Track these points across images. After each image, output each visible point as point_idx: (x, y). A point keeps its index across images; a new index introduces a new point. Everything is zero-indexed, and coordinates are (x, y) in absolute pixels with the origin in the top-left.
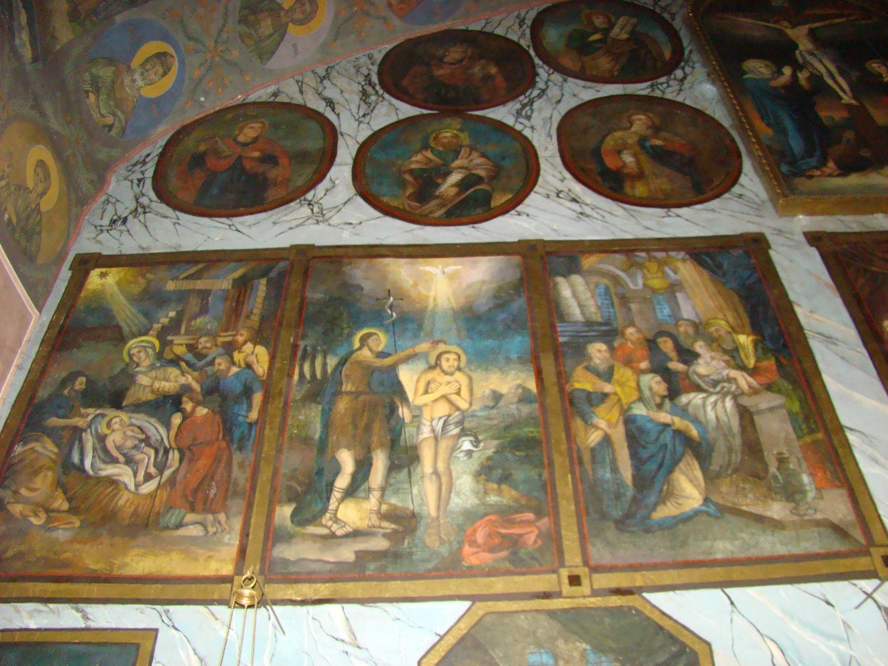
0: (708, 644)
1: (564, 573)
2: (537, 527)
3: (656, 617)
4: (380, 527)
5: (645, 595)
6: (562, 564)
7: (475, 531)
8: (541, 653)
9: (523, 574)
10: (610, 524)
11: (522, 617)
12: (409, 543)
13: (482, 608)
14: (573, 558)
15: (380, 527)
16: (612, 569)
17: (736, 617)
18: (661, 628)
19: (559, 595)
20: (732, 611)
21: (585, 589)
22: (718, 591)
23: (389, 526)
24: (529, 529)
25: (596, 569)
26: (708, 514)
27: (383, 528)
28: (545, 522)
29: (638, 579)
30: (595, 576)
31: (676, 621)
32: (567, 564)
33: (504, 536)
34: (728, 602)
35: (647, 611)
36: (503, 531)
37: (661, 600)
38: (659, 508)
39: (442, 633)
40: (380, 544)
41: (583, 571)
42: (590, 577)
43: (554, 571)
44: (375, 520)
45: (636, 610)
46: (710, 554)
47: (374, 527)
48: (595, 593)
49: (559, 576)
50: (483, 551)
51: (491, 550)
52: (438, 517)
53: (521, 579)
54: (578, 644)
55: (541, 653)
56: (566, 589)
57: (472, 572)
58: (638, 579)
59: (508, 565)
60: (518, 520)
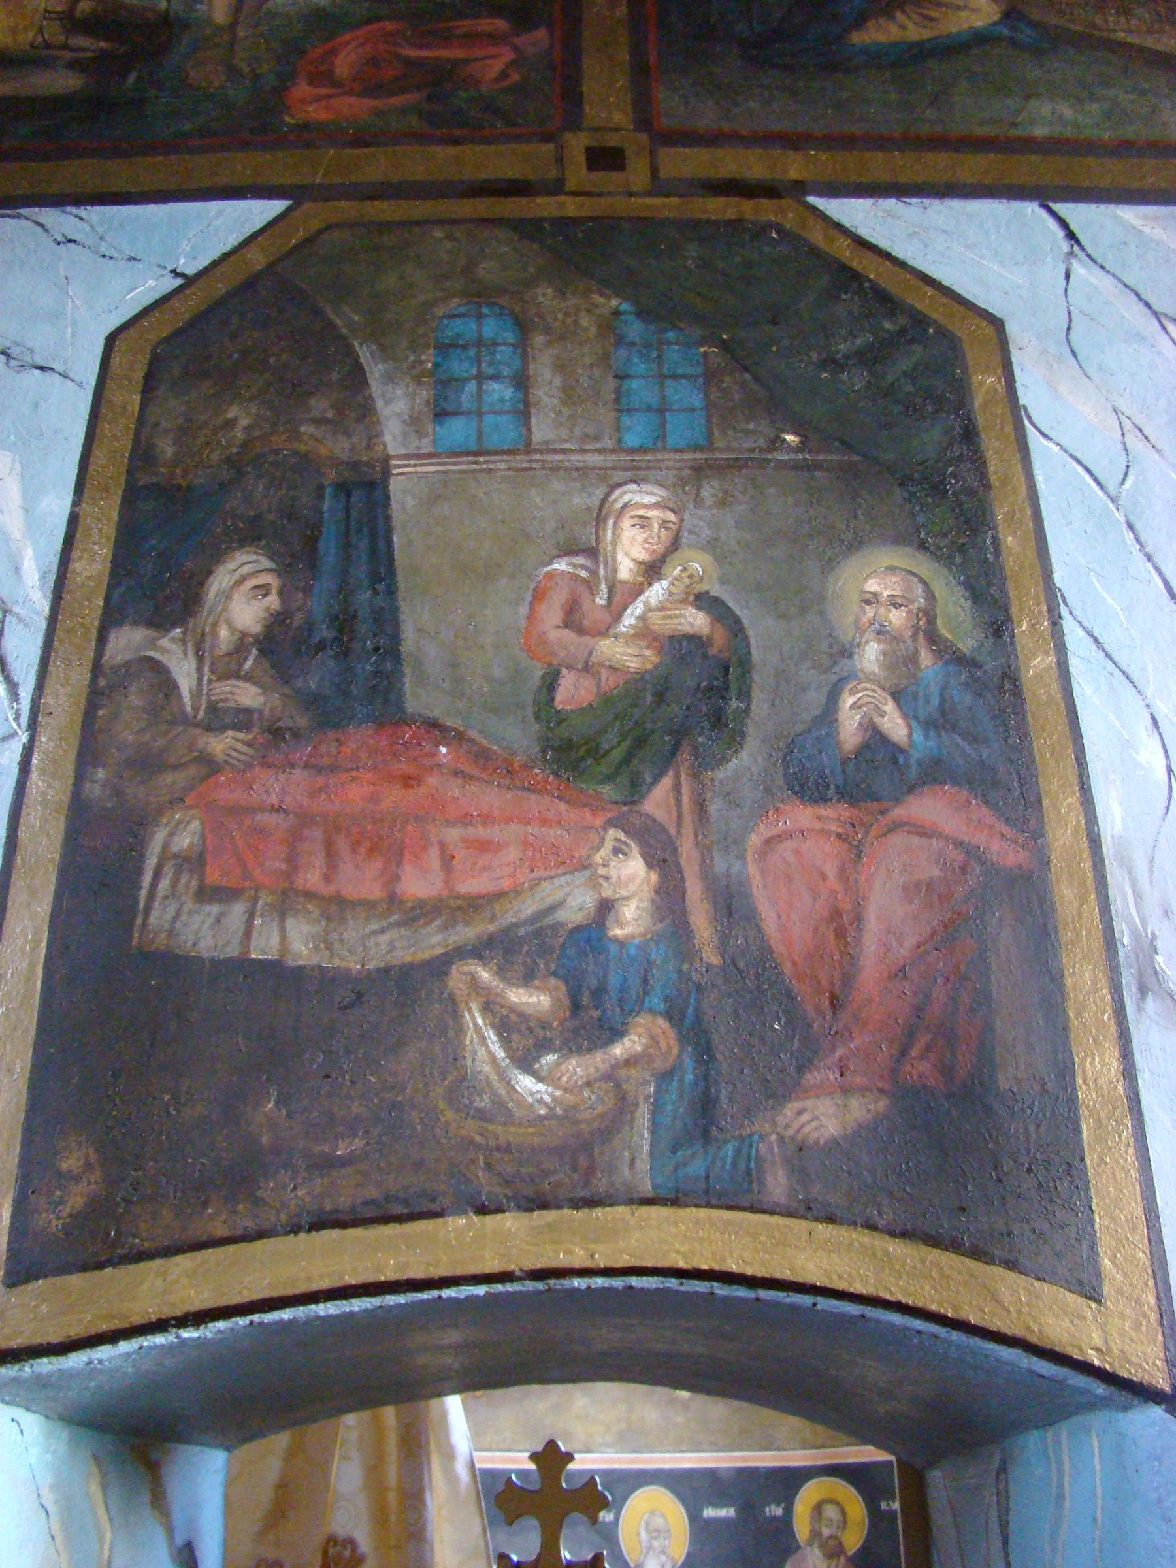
0: (998, 324)
1: (577, 144)
2: (515, 48)
3: (842, 249)
4: (65, 47)
5: (812, 200)
6: (574, 122)
7: (334, 52)
8: (480, 317)
9: (456, 142)
10: (655, 407)
11: (438, 233)
12: (139, 79)
13: (315, 215)
14: (607, 104)
15: (65, 47)
16: (713, 139)
17: (1080, 270)
18: (856, 276)
19: (557, 188)
20: (1071, 253)
21: (637, 173)
22: (1031, 209)
23: (88, 44)
24: (494, 50)
25: (671, 138)
26: (1013, 43)
27: (71, 49)
28: (538, 40)
29: (794, 167)
30: (663, 153)
31: (902, 264)
32: (587, 123)
33: (409, 62)
34: (1061, 234)
35: (817, 236)
36: (413, 53)
37: (858, 214)
38: (871, 24)
39: (190, 271)
40: (63, 82)
41: (634, 143)
42: (652, 154)
43: (547, 138)
44: (54, 32)
45: (780, 230)
46: (1014, 125)
47: (47, 46)
48: (658, 187)
49: (561, 148)
50: (350, 93)
51: (373, 90)
52: (233, 25)
53: (442, 152)
54: (597, 299)
55: (480, 317)
56: (578, 173)
57: (308, 136)
58: (794, 167)
59: (414, 121)
60: (459, 32)
